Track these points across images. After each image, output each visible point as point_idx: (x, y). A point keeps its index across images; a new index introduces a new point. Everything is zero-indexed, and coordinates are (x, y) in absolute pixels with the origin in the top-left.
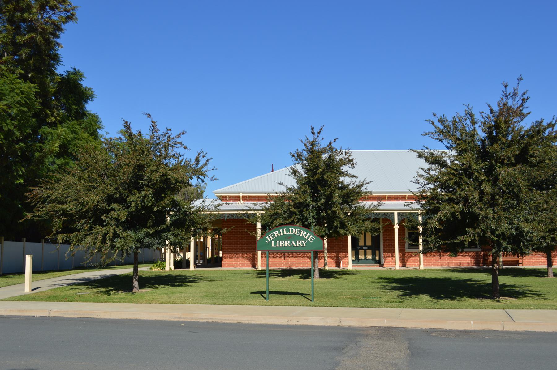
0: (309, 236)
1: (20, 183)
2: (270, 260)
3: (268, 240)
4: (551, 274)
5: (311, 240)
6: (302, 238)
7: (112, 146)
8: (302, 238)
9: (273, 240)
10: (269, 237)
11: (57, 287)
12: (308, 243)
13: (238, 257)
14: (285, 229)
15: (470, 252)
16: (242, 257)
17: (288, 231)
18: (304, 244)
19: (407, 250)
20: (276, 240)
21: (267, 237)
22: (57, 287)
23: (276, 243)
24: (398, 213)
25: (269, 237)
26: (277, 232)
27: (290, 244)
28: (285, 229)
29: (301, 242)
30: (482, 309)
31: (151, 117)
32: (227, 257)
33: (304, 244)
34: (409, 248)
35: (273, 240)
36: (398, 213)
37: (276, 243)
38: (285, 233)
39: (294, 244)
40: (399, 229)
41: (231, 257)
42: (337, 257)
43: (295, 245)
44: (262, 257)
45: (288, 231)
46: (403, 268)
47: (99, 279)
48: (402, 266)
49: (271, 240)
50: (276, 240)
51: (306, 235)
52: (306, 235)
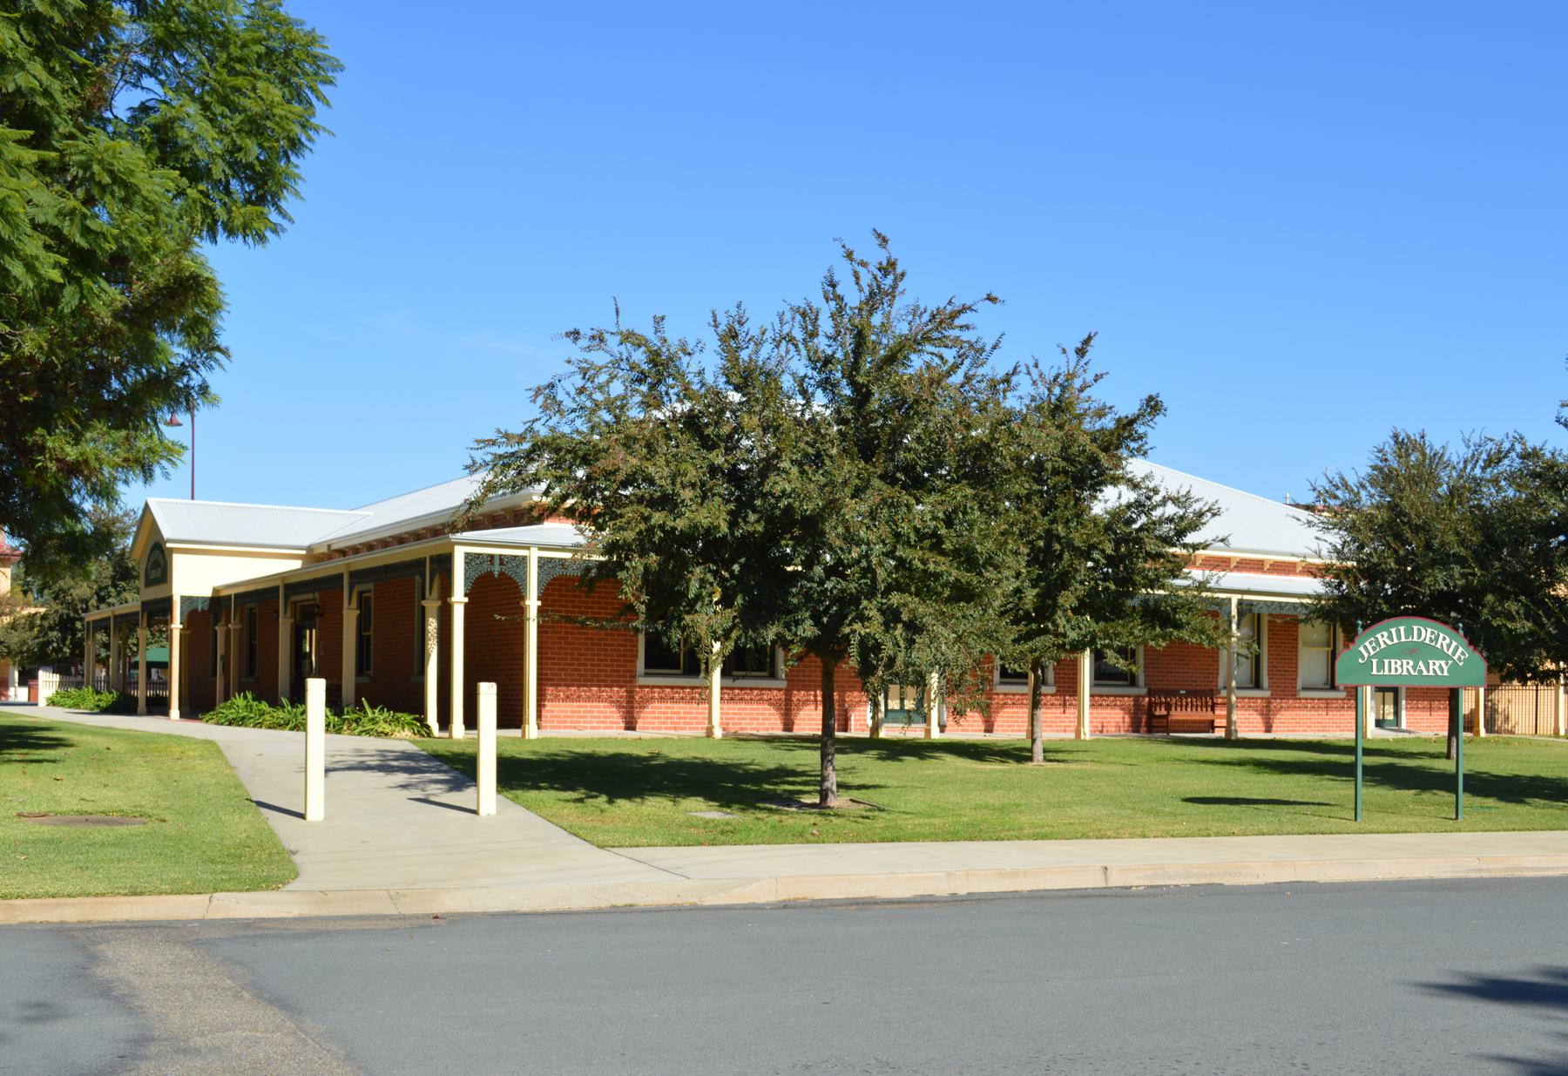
0: (1456, 649)
4: (1039, 754)
6: (1440, 654)
8: (1440, 654)
11: (45, 830)
12: (1454, 668)
13: (588, 700)
14: (1402, 628)
15: (683, 688)
16: (599, 699)
17: (1409, 632)
19: (642, 681)
20: (1382, 655)
22: (45, 830)
23: (1381, 666)
24: (467, 555)
27: (1414, 668)
28: (1402, 628)
30: (142, 894)
31: (890, 246)
32: (556, 698)
34: (646, 675)
35: (1374, 656)
36: (467, 555)
37: (1381, 666)
40: (467, 606)
41: (567, 698)
42: (788, 701)
44: (1092, 706)
45: (1409, 632)
46: (630, 734)
48: (627, 728)
50: (1382, 655)
51: (1449, 646)
52: (1449, 646)
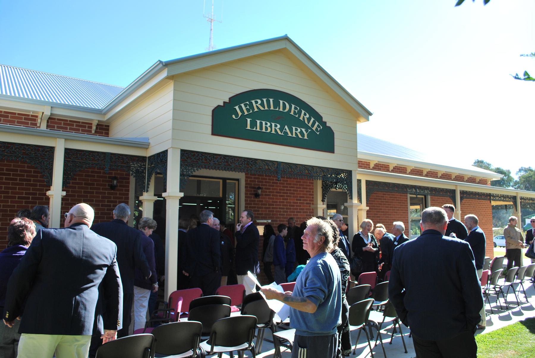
1: (382, 254)
2: (505, 249)
3: (237, 114)
5: (316, 129)
6: (302, 124)
7: (202, 341)
8: (302, 124)
9: (248, 116)
10: (241, 108)
14: (271, 100)
18: (306, 134)
21: (237, 108)
23: (253, 124)
25: (241, 108)
26: (308, 116)
27: (281, 129)
28: (271, 100)
29: (299, 130)
33: (306, 134)
35: (248, 116)
37: (253, 124)
38: (272, 108)
39: (288, 130)
43: (290, 135)
47: (131, 309)
49: (244, 117)
52: (262, 104)
